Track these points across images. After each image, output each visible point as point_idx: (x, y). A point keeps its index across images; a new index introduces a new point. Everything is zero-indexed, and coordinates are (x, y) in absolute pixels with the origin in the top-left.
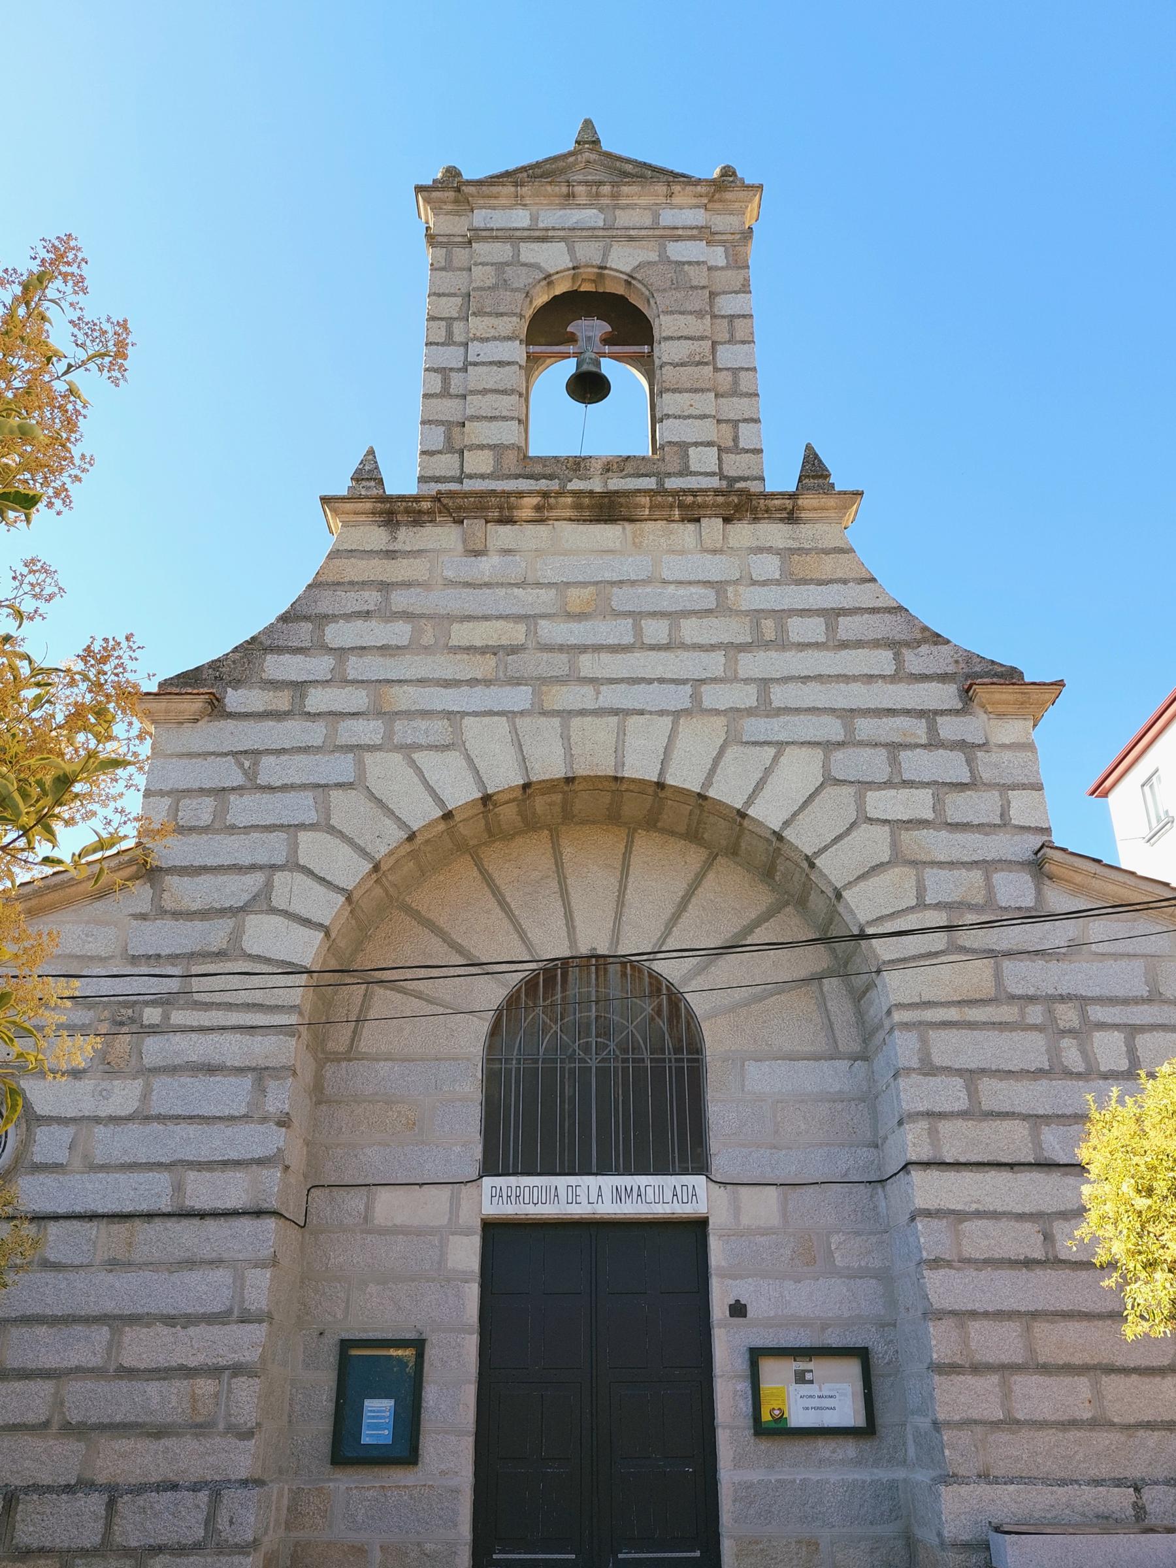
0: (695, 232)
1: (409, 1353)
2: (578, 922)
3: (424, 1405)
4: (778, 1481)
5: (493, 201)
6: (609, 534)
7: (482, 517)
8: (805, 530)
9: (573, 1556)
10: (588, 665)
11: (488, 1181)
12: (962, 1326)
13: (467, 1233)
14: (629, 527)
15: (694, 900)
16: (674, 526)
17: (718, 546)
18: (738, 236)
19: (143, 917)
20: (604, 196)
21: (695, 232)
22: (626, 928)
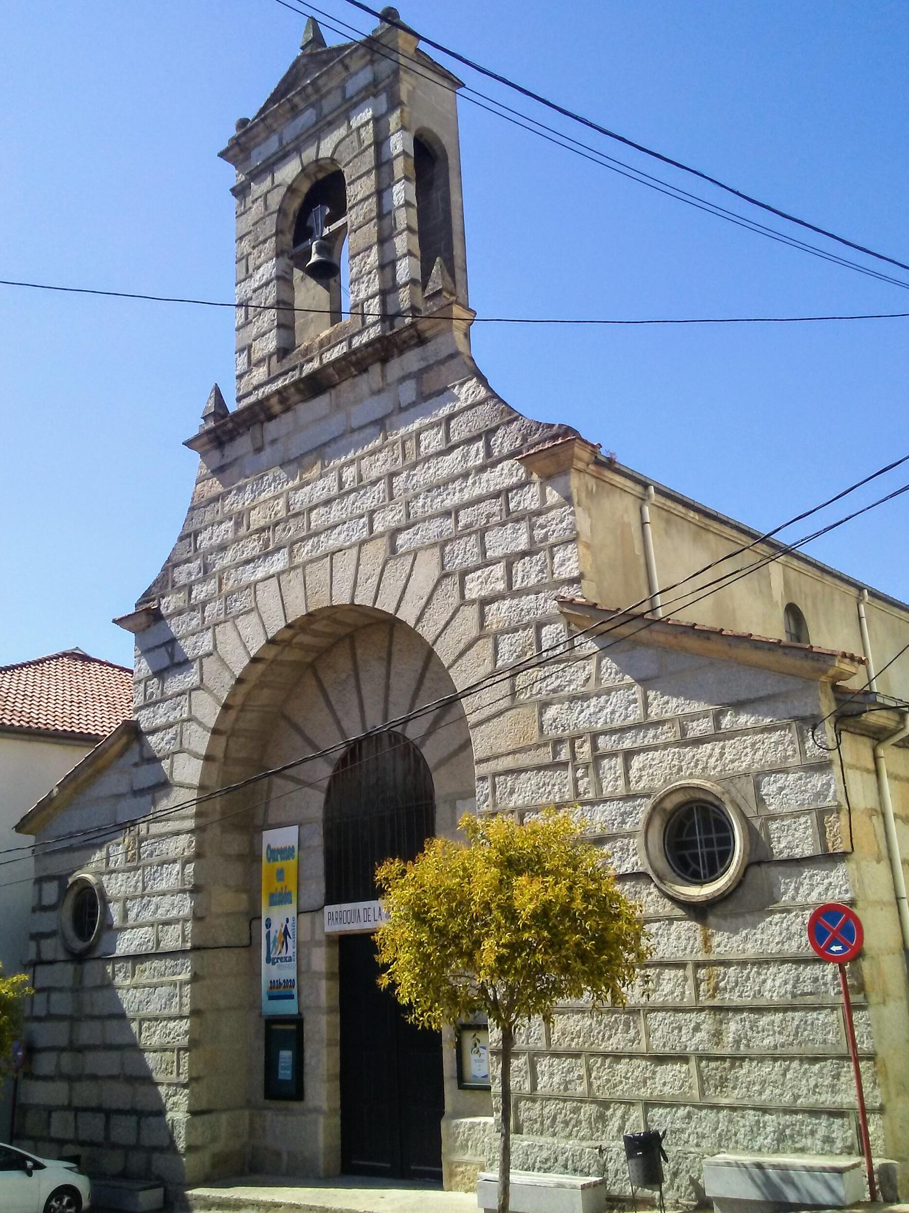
0: (363, 94)
1: (293, 1027)
2: (366, 708)
3: (305, 1062)
4: (471, 1123)
5: (258, 140)
6: (322, 403)
7: (255, 423)
8: (431, 347)
9: (388, 1165)
10: (317, 518)
11: (328, 909)
12: (71, 1042)
13: (318, 944)
14: (333, 392)
15: (428, 675)
16: (357, 379)
17: (381, 385)
18: (392, 77)
19: (136, 765)
20: (312, 95)
21: (363, 94)
22: (391, 706)
